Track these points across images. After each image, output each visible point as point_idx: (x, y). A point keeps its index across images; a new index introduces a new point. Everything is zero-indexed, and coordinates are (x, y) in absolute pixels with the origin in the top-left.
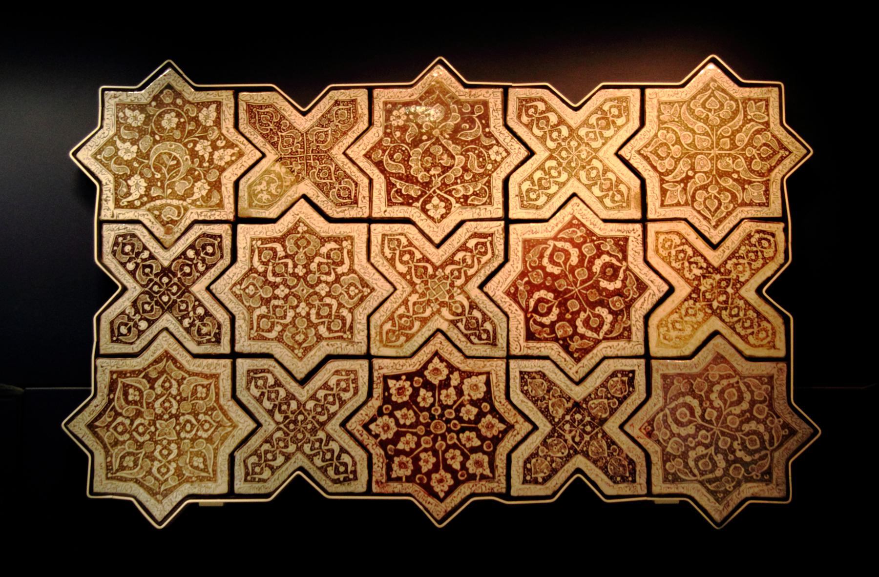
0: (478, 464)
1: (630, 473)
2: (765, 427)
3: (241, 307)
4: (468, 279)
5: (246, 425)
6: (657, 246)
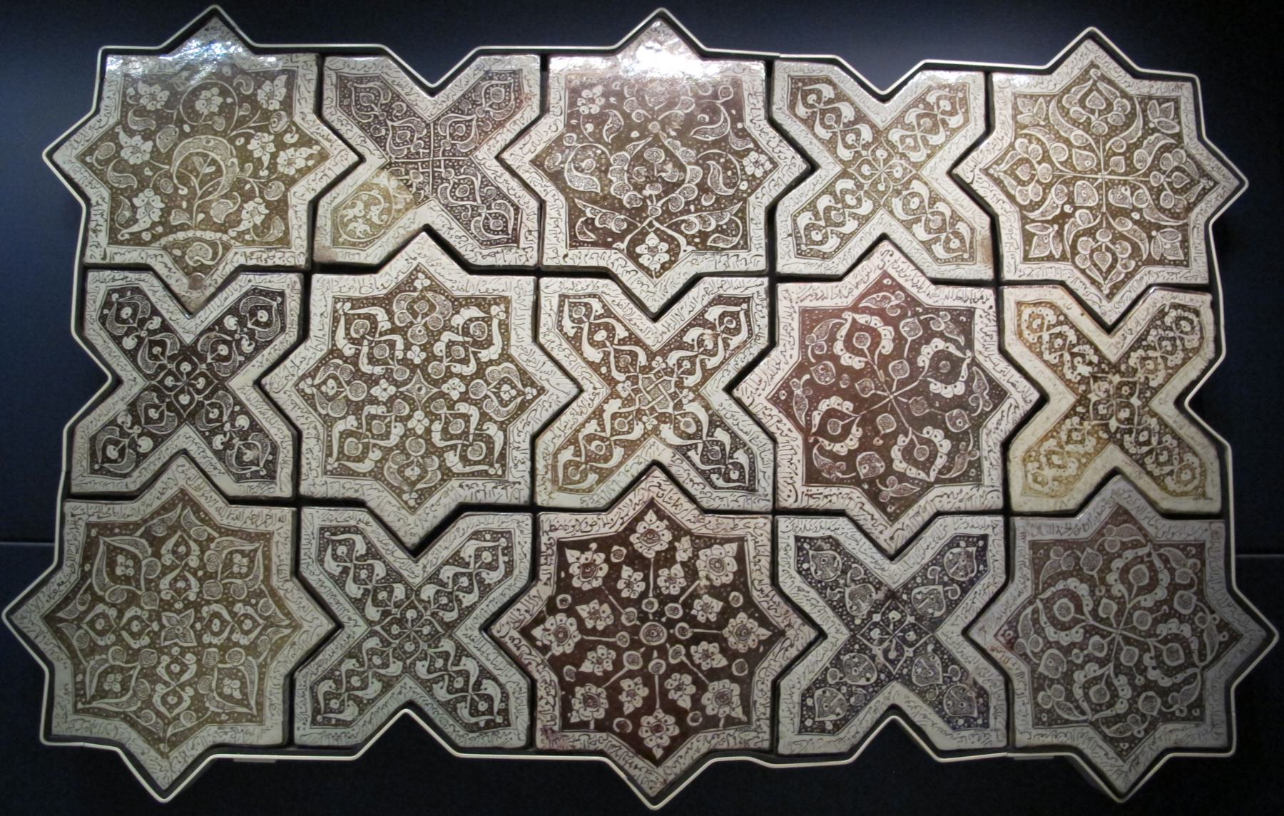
0: (722, 698)
1: (979, 712)
2: (1193, 630)
3: (313, 418)
4: (708, 374)
5: (319, 625)
6: (1019, 326)
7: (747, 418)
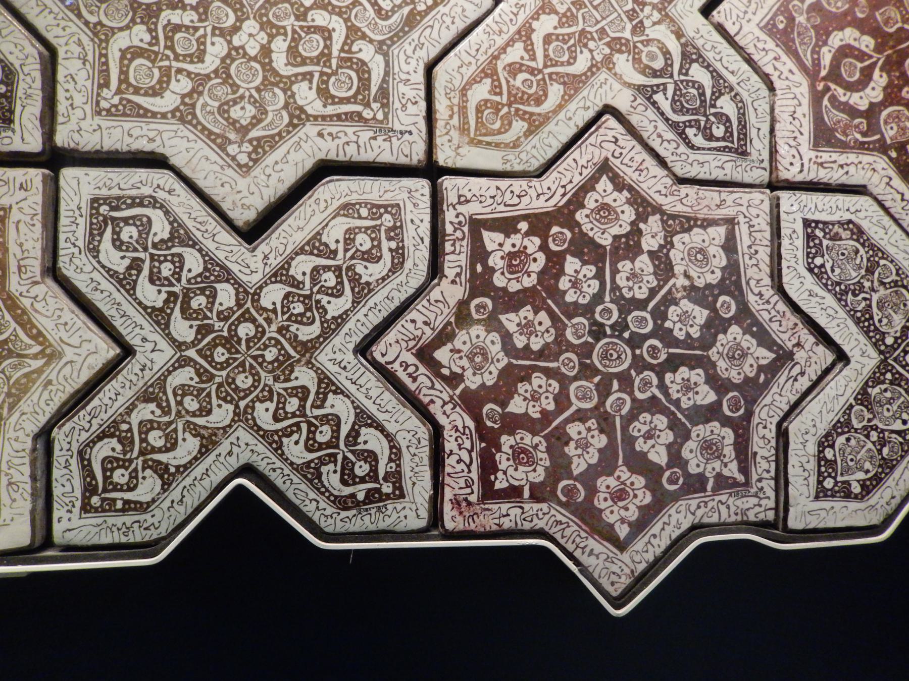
0: (710, 448)
7: (732, 51)
